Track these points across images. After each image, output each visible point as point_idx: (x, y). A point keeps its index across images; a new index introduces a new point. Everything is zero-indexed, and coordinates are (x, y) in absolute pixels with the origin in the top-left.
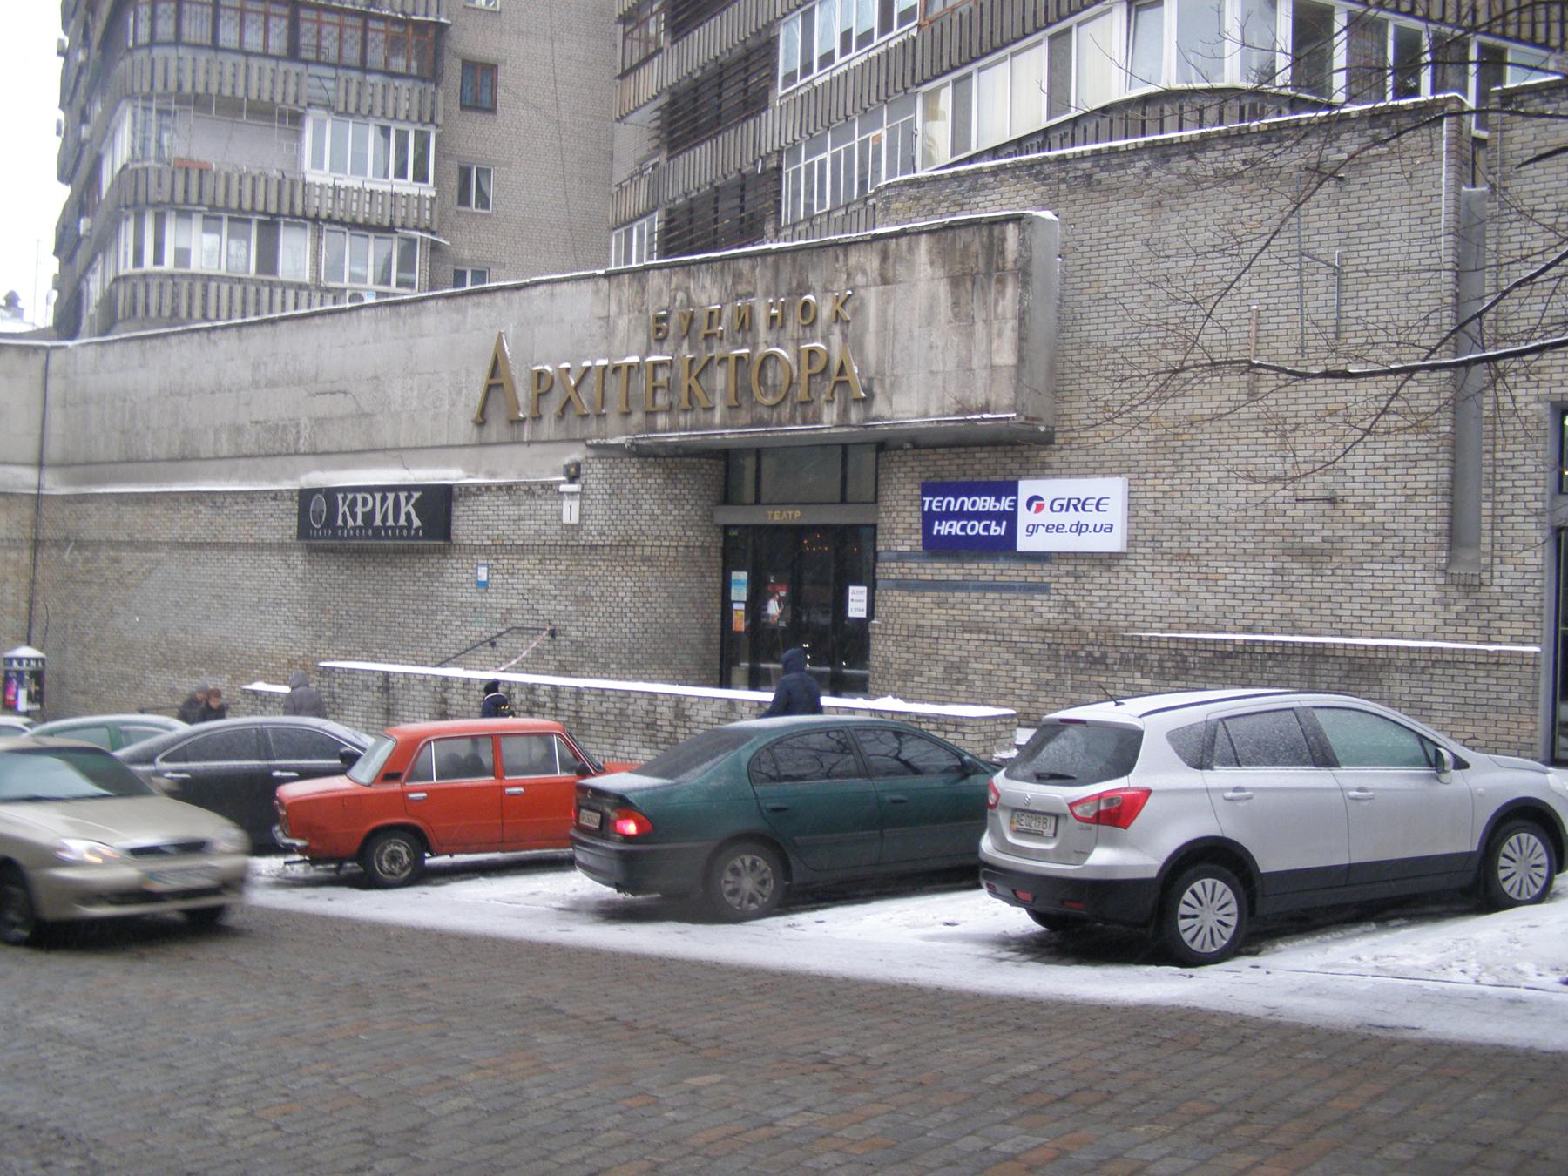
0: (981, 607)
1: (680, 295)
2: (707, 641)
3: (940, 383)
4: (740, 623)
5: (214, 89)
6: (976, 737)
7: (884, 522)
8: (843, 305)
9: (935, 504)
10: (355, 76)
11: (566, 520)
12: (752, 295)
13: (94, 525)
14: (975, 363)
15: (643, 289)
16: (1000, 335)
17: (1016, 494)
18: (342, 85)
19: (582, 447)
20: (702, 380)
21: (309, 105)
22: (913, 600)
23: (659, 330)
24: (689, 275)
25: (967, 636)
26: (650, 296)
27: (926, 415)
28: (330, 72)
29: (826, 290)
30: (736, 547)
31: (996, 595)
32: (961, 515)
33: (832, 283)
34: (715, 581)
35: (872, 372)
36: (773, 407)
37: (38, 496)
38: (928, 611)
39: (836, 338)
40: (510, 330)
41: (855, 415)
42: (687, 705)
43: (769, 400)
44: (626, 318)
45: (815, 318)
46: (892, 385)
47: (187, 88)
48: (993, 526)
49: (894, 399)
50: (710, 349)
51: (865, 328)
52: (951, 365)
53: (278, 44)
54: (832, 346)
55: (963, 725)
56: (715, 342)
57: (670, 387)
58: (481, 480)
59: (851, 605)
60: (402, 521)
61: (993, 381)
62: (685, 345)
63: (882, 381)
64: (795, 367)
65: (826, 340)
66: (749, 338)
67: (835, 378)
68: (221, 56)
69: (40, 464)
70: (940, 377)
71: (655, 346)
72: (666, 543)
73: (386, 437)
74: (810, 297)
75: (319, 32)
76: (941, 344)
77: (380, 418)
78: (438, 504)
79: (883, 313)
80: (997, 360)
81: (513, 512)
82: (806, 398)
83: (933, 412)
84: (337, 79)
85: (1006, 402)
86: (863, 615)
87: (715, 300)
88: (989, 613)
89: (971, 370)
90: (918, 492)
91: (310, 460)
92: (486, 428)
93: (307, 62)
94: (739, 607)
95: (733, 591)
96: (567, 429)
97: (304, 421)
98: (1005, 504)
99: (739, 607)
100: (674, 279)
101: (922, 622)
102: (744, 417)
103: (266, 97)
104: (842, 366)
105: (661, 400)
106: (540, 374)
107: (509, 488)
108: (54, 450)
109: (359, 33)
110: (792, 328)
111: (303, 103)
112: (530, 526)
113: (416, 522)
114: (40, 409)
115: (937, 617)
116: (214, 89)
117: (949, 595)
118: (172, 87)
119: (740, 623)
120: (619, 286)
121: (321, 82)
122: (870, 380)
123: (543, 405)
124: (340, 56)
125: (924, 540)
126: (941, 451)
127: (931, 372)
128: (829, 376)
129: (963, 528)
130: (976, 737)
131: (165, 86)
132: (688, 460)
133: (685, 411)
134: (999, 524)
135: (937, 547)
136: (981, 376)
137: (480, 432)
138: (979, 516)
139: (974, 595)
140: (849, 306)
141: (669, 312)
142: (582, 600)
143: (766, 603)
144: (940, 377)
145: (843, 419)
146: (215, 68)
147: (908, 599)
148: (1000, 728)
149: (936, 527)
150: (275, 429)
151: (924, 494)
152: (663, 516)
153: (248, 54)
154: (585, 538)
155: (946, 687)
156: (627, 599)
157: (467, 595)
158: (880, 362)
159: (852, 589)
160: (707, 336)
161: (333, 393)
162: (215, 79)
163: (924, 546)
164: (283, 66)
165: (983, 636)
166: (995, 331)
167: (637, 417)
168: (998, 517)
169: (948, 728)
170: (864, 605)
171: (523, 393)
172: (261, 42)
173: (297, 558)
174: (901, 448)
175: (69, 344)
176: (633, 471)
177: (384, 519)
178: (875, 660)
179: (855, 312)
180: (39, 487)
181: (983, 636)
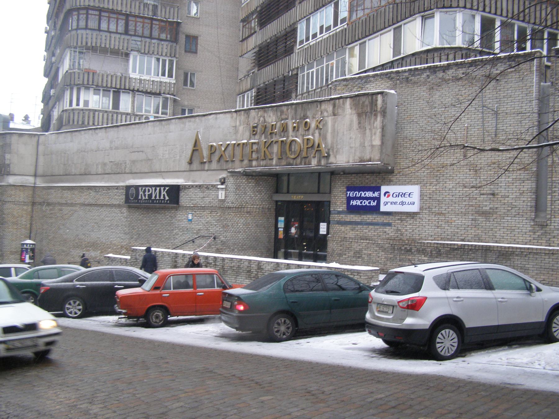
0: (367, 231)
1: (262, 119)
4: (281, 235)
5: (98, 45)
7: (333, 200)
8: (319, 123)
9: (351, 194)
10: (148, 40)
11: (220, 198)
12: (287, 119)
13: (54, 197)
14: (366, 144)
16: (375, 134)
19: (226, 172)
21: (132, 50)
22: (343, 228)
23: (254, 131)
24: (265, 111)
25: (362, 241)
26: (251, 119)
27: (348, 162)
28: (139, 39)
29: (313, 118)
32: (360, 198)
35: (329, 147)
36: (294, 159)
38: (348, 232)
39: (317, 135)
40: (201, 130)
41: (323, 162)
43: (293, 156)
45: (309, 127)
46: (337, 152)
47: (89, 44)
48: (372, 202)
49: (337, 157)
50: (272, 138)
51: (327, 131)
52: (358, 144)
53: (121, 29)
54: (315, 137)
55: (360, 273)
56: (274, 136)
57: (258, 151)
59: (321, 230)
60: (162, 198)
62: (263, 136)
63: (333, 150)
65: (313, 135)
66: (286, 135)
67: (316, 149)
68: (101, 33)
69: (35, 176)
70: (354, 148)
72: (255, 207)
73: (157, 167)
74: (308, 120)
75: (136, 25)
76: (354, 137)
79: (333, 126)
80: (374, 143)
81: (201, 195)
82: (306, 156)
84: (141, 41)
86: (325, 233)
93: (131, 35)
94: (281, 230)
97: (128, 162)
98: (376, 194)
100: (260, 113)
101: (346, 236)
102: (284, 162)
104: (319, 145)
106: (212, 146)
107: (200, 186)
108: (40, 171)
111: (130, 50)
112: (207, 200)
113: (167, 198)
114: (35, 156)
115: (352, 234)
116: (98, 45)
118: (84, 44)
119: (281, 235)
122: (329, 150)
123: (212, 157)
124: (143, 33)
129: (361, 203)
131: (82, 43)
133: (263, 160)
135: (352, 209)
136: (368, 149)
138: (367, 199)
139: (365, 227)
142: (225, 226)
143: (290, 228)
144: (354, 148)
145: (319, 164)
146: (99, 37)
148: (373, 274)
150: (117, 164)
151: (348, 190)
152: (255, 197)
153: (110, 32)
154: (227, 205)
155: (354, 259)
156: (241, 226)
157: (184, 224)
158: (332, 143)
159: (321, 224)
160: (271, 133)
162: (99, 41)
164: (123, 37)
165: (368, 241)
166: (373, 133)
167: (246, 162)
168: (374, 199)
169: (355, 274)
170: (325, 230)
171: (205, 153)
172: (115, 28)
173: (124, 210)
175: (46, 133)
177: (156, 197)
178: (329, 249)
179: (324, 125)
180: (35, 183)
181: (368, 241)
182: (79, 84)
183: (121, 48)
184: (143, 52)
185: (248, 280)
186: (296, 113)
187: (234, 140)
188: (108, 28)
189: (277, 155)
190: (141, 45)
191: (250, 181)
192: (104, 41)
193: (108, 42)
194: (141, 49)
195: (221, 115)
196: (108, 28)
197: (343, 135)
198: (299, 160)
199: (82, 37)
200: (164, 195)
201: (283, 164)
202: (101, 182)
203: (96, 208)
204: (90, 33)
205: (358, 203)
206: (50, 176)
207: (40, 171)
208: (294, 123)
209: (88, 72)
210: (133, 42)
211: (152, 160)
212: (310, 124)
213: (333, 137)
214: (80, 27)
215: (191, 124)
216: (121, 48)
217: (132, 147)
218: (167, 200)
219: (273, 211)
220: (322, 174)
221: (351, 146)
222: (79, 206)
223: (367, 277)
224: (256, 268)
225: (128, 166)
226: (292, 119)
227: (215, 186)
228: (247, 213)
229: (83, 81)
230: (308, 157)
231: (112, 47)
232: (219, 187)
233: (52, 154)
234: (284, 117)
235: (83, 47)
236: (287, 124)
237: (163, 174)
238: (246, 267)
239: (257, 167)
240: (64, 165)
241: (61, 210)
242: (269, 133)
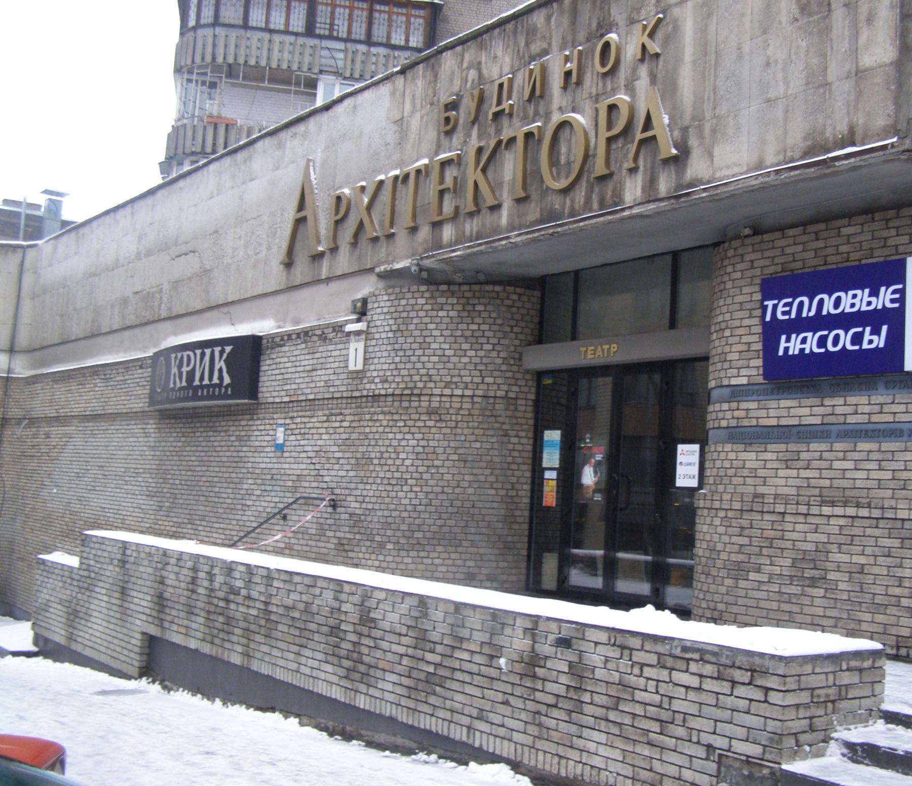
0: (849, 465)
1: (473, 74)
2: (509, 519)
3: (780, 114)
4: (550, 497)
5: (241, 60)
6: (791, 699)
7: (717, 346)
8: (651, 35)
9: (780, 309)
10: (362, 48)
11: (352, 367)
12: (546, 52)
13: (41, 403)
14: (834, 72)
15: (436, 76)
16: (870, 20)
17: (902, 279)
18: (350, 56)
19: (373, 278)
20: (490, 174)
21: (321, 72)
22: (750, 457)
23: (447, 120)
24: (482, 47)
25: (827, 510)
26: (442, 84)
27: (760, 165)
28: (341, 46)
29: (632, 22)
30: (556, 400)
31: (873, 446)
32: (821, 322)
33: (638, 10)
34: (523, 443)
35: (687, 120)
36: (565, 191)
37: (7, 379)
38: (769, 472)
39: (643, 83)
40: (318, 156)
41: (664, 186)
42: (372, 603)
43: (563, 183)
44: (418, 116)
45: (617, 62)
46: (714, 131)
47: (220, 59)
48: (867, 337)
49: (717, 151)
50: (498, 131)
51: (679, 60)
52: (797, 82)
53: (298, 22)
54: (638, 95)
55: (765, 673)
56: (505, 121)
57: (457, 188)
58: (289, 328)
59: (680, 470)
60: (216, 380)
61: (860, 94)
62: (475, 133)
63: (700, 128)
64: (592, 134)
65: (630, 88)
66: (542, 111)
67: (639, 136)
68: (249, 34)
69: (11, 350)
70: (781, 105)
71: (445, 142)
72: (458, 392)
73: (219, 294)
74: (613, 36)
75: (333, 13)
76: (781, 56)
77: (216, 273)
78: (248, 354)
79: (702, 32)
80: (867, 61)
81: (307, 362)
82: (605, 171)
83: (770, 159)
84: (345, 51)
85: (881, 122)
86: (694, 483)
87: (506, 69)
88: (862, 475)
89: (826, 85)
90: (758, 296)
91: (168, 325)
92: (293, 270)
93: (321, 37)
94: (550, 475)
95: (545, 456)
96: (359, 258)
97: (166, 286)
98: (885, 298)
99: (550, 475)
100: (467, 57)
101: (761, 490)
102: (533, 211)
103: (284, 66)
104: (648, 118)
105: (448, 207)
106: (339, 198)
107: (305, 335)
108: (23, 340)
109: (365, 13)
110: (590, 84)
111: (316, 70)
112: (322, 375)
113: (227, 380)
114: (14, 301)
115: (784, 482)
116: (241, 60)
117: (803, 447)
118: (208, 59)
119: (550, 497)
120: (414, 79)
121: (335, 54)
122: (685, 130)
123: (340, 234)
124: (349, 32)
125: (765, 366)
126: (791, 232)
127: (768, 101)
128: (630, 134)
129: (822, 342)
130: (791, 699)
131: (203, 59)
132: (490, 288)
133: (471, 214)
134: (876, 331)
135: (785, 375)
136: (842, 90)
137: (288, 273)
138: (845, 321)
139: (838, 446)
140: (660, 35)
141: (460, 97)
142: (362, 463)
143: (580, 474)
144: (781, 105)
145: (650, 195)
146: (244, 43)
147: (743, 456)
148: (846, 678)
149: (783, 344)
150: (146, 297)
151: (766, 296)
152: (456, 356)
153: (272, 31)
154: (369, 387)
155: (793, 590)
156: (413, 462)
157: (266, 461)
158: (699, 100)
159: (680, 447)
160: (497, 115)
161: (186, 254)
162: (242, 52)
163: (766, 376)
164: (301, 40)
165: (851, 511)
166: (863, 16)
167: (425, 232)
168: (873, 319)
169: (738, 675)
170: (695, 470)
171: (324, 224)
172: (283, 21)
173: (151, 427)
174: (737, 237)
175: (39, 242)
176: (422, 301)
177: (202, 378)
178: (700, 548)
179: (667, 40)
180: (9, 371)
181: (851, 511)
182: (193, 153)
183: (295, 67)
184: (348, 75)
185: (329, 668)
186: (573, 23)
187: (396, 168)
188: (267, 21)
189: (512, 190)
190: (345, 59)
191: (442, 300)
192: (254, 52)
193: (265, 53)
194: (345, 68)
195: (367, 94)
196: (267, 21)
197: (740, 56)
198: (580, 194)
199: (204, 45)
200: (221, 370)
201: (531, 218)
202: (117, 352)
203: (103, 425)
204: (223, 35)
205: (810, 343)
206: (39, 351)
207: (23, 340)
208: (567, 59)
209: (216, 124)
210: (325, 53)
211: (210, 271)
212: (619, 50)
213: (702, 75)
214: (202, 22)
215: (296, 142)
216: (295, 67)
217: (176, 244)
218: (228, 385)
219: (526, 411)
220: (684, 257)
221: (772, 94)
222: (76, 422)
223: (804, 698)
224: (354, 617)
225: (165, 299)
226: (562, 48)
227: (346, 334)
228: (428, 413)
229: (203, 146)
230: (610, 176)
231: (274, 65)
232: (350, 328)
233: (45, 293)
234: (535, 48)
235: (206, 67)
236: (544, 70)
237: (233, 309)
238: (326, 611)
239: (455, 243)
240: (62, 316)
241: (48, 436)
242: (490, 116)
